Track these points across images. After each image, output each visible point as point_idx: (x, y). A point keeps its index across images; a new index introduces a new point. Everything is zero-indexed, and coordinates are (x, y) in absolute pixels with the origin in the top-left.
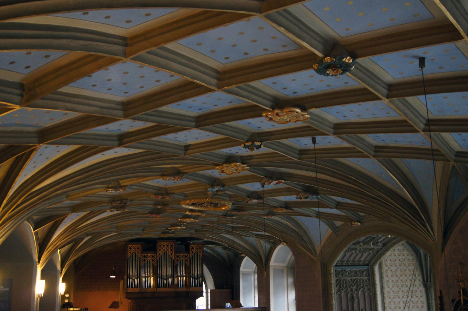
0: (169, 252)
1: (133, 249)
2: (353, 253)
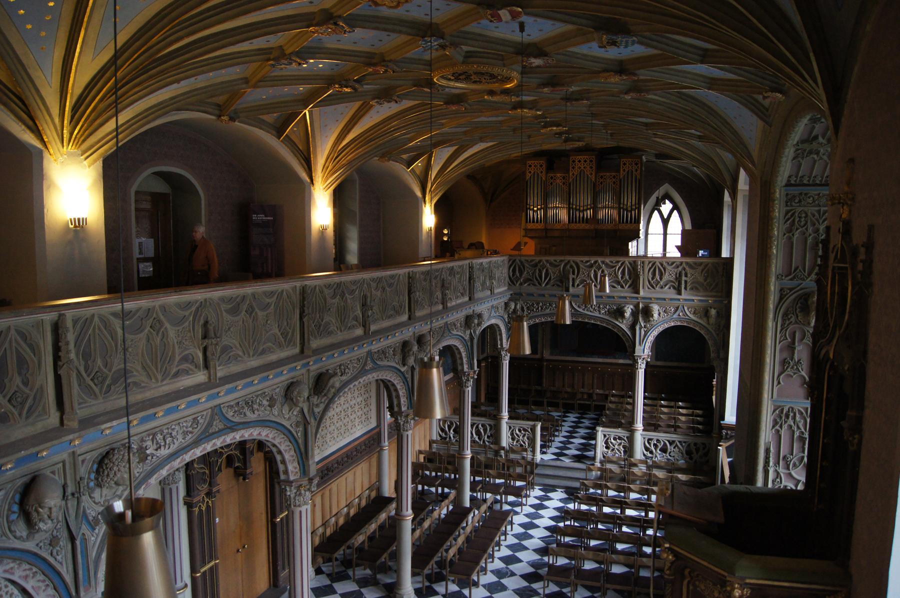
1: (536, 168)
2: (815, 162)
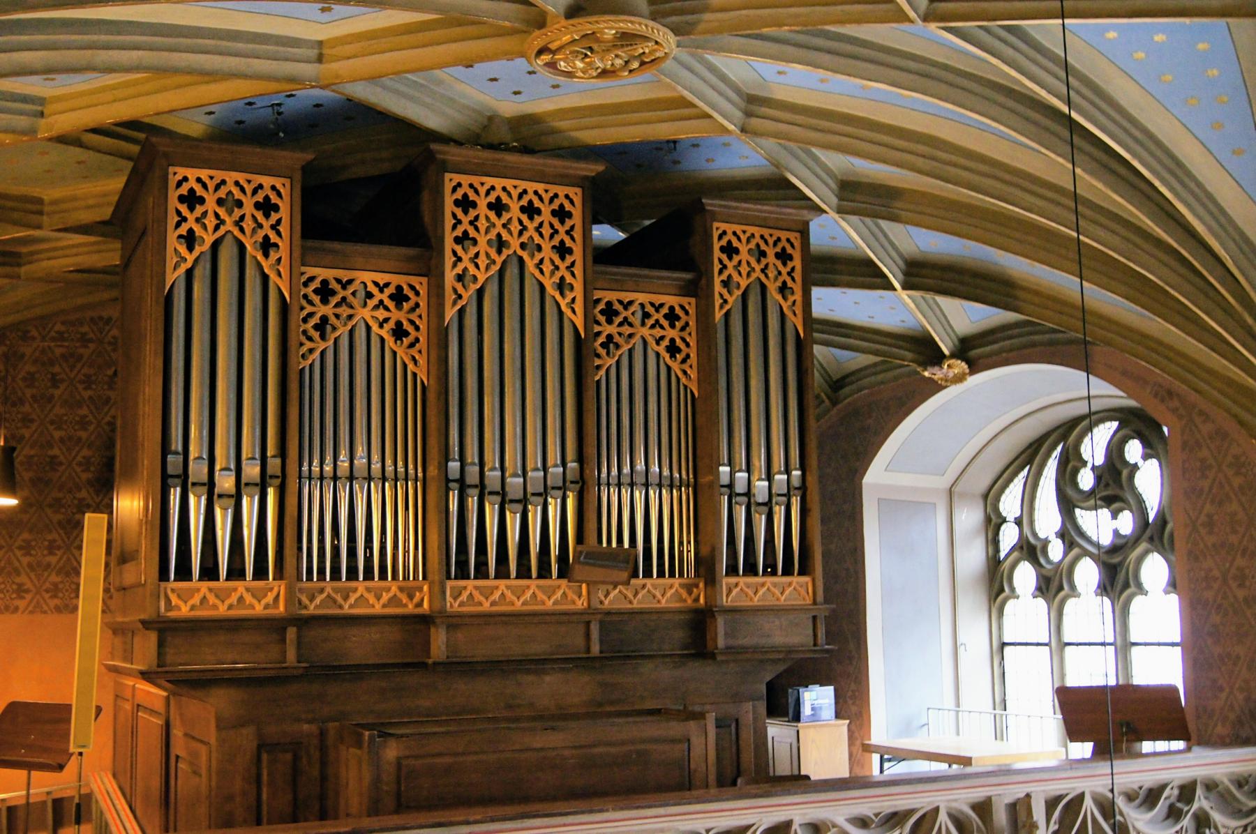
0: (544, 269)
1: (234, 217)
